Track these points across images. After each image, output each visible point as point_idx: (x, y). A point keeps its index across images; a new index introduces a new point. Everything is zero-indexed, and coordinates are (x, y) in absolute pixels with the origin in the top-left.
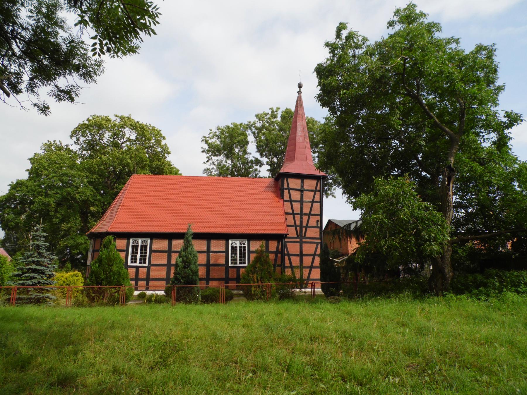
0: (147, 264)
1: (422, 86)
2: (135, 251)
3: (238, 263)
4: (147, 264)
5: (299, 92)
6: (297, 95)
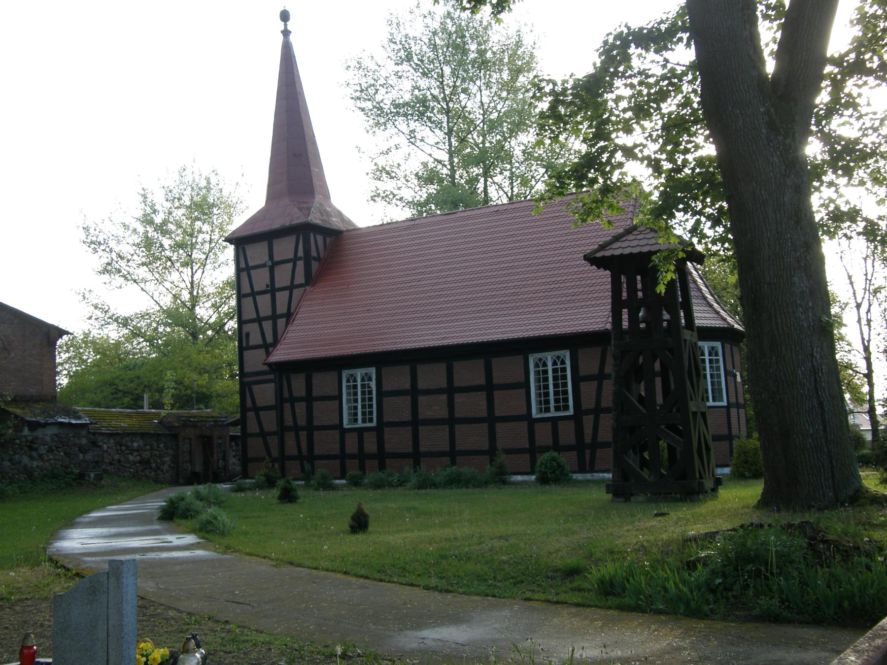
0: (571, 412)
1: (640, 102)
2: (561, 393)
3: (552, 409)
4: (571, 412)
5: (286, 33)
6: (281, 37)
